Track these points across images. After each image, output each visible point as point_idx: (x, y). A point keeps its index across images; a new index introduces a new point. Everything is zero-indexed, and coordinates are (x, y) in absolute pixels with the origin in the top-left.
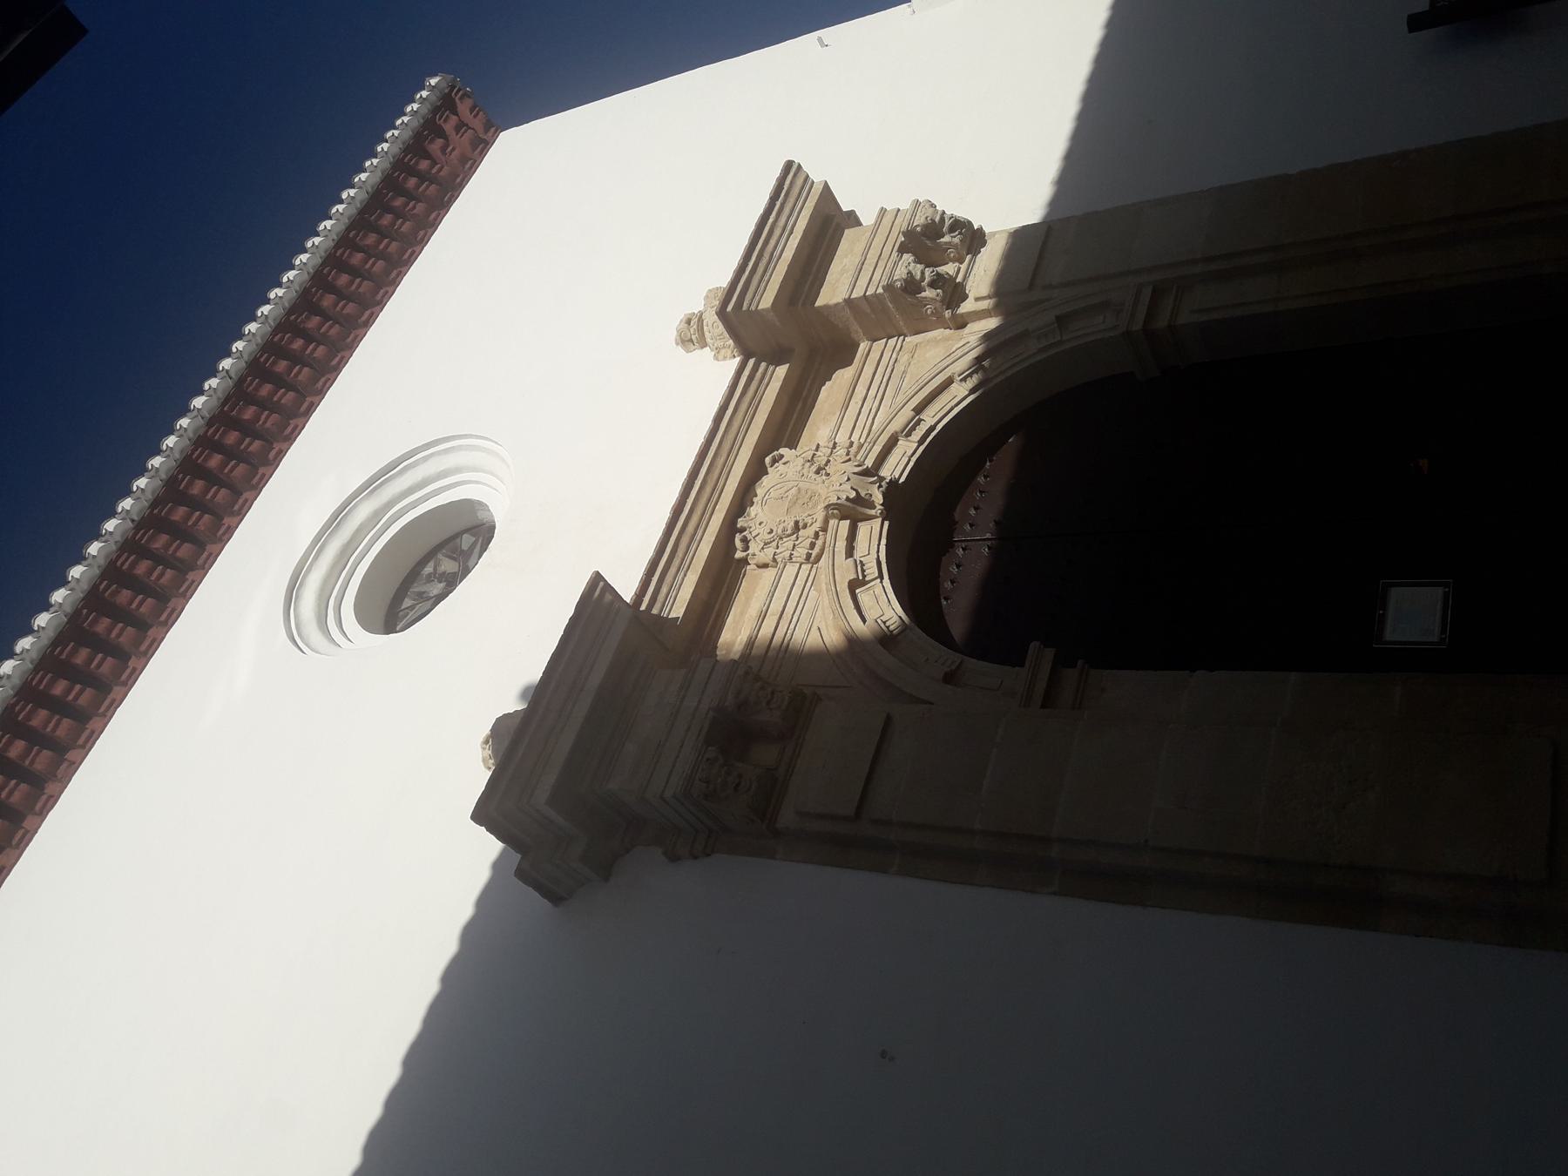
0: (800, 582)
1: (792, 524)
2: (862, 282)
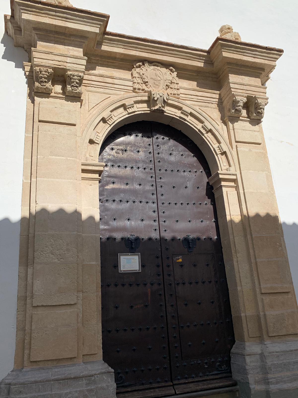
0: (126, 88)
1: (147, 81)
2: (236, 86)
